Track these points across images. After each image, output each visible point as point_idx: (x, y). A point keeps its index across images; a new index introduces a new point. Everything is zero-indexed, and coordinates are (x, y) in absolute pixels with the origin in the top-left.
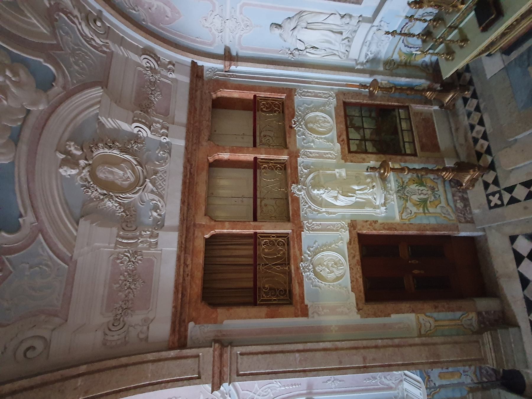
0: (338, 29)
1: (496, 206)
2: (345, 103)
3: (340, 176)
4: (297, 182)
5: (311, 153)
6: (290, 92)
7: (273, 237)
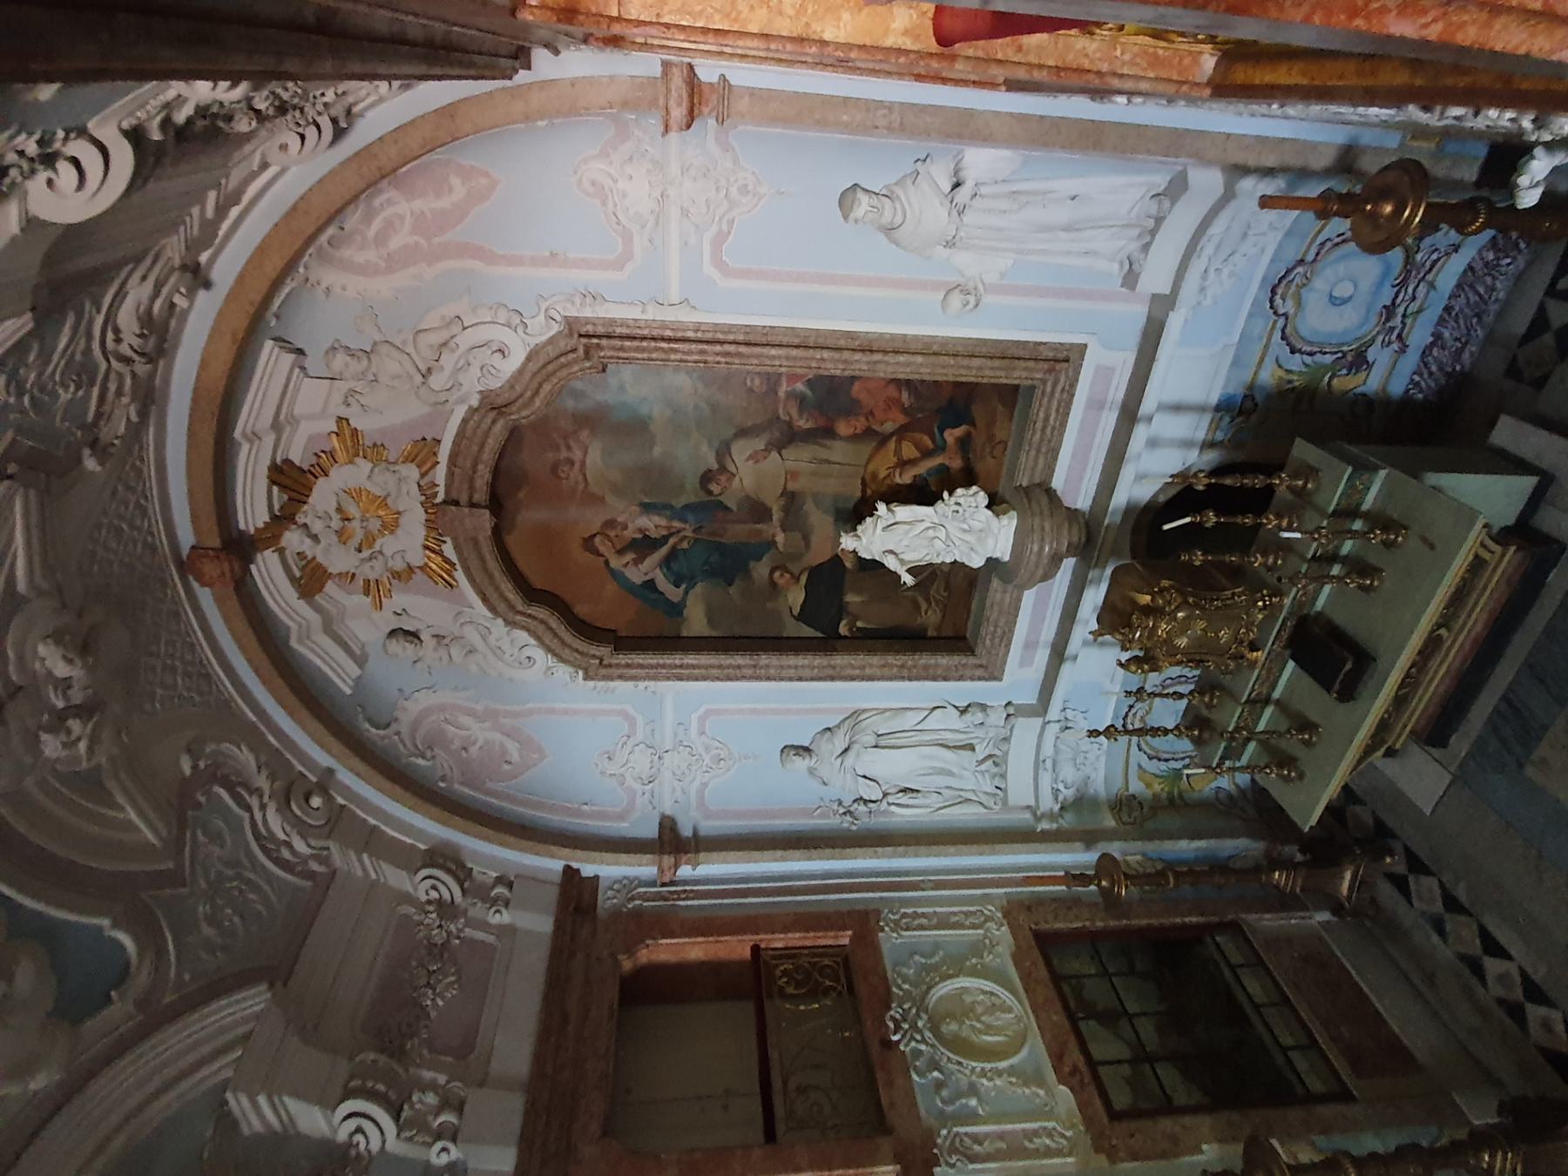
0: (962, 739)
6: (864, 922)
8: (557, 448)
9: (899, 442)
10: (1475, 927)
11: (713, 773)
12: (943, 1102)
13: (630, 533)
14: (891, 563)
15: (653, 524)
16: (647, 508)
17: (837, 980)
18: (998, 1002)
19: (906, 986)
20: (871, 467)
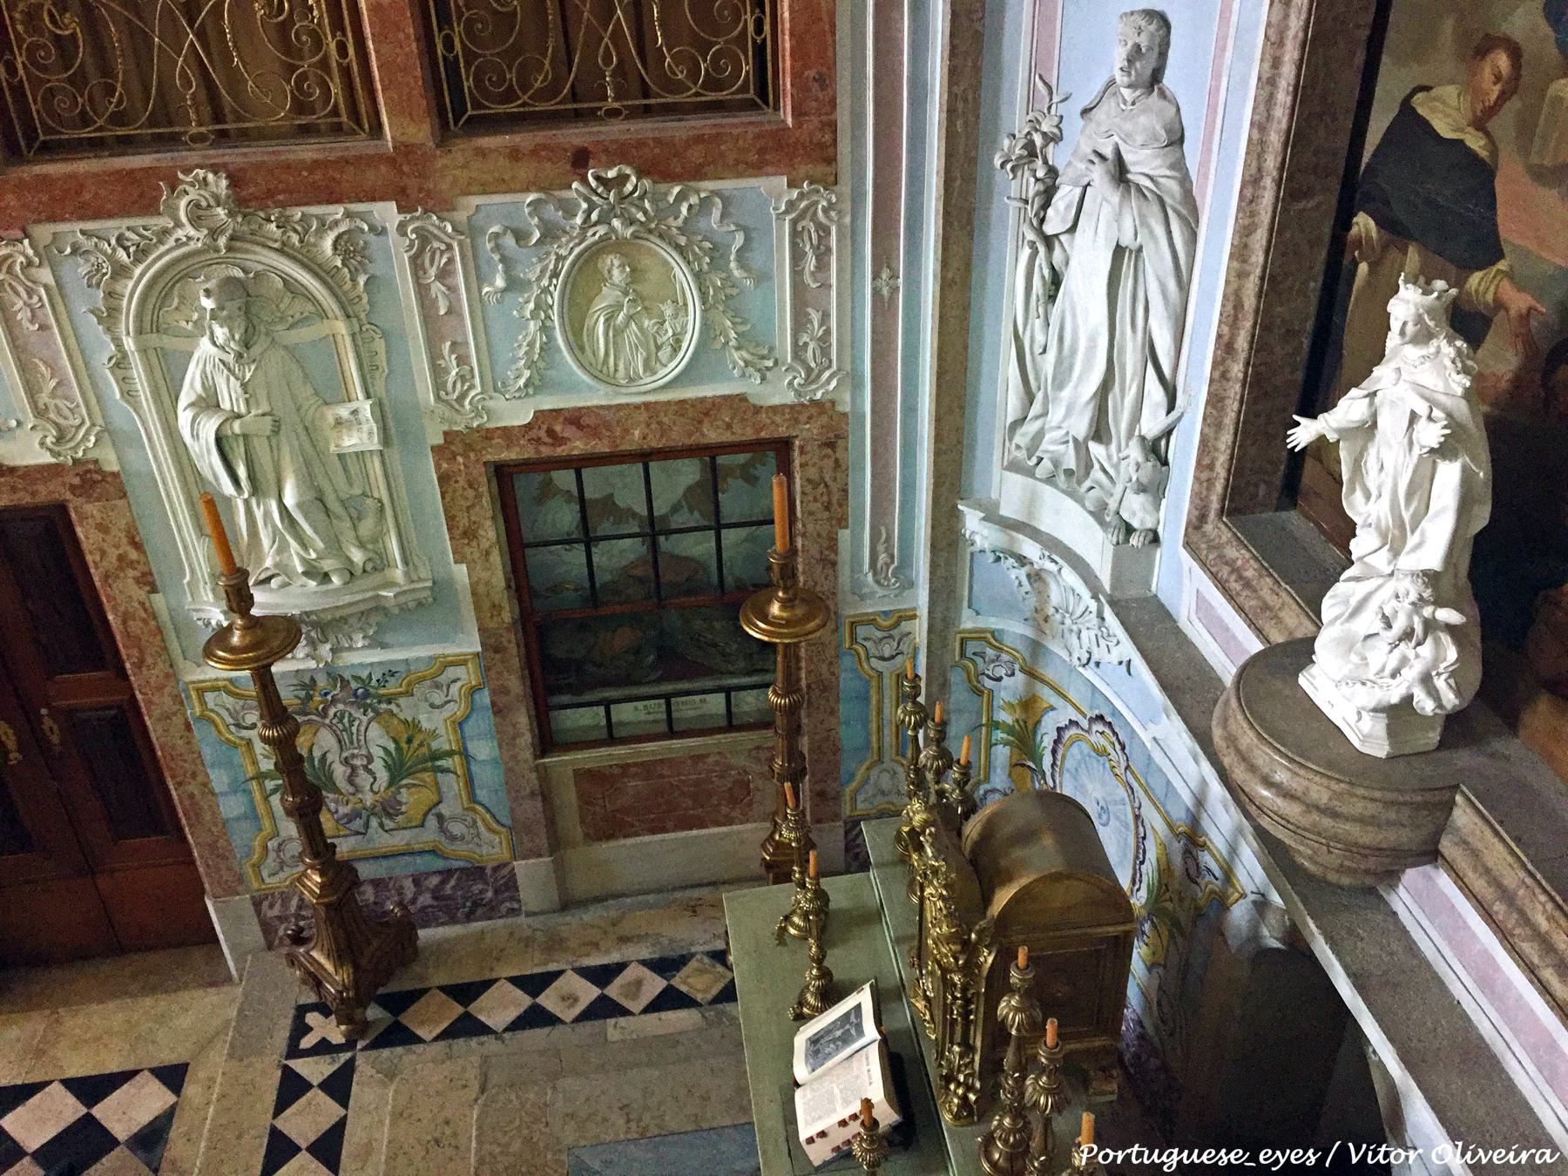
0: (1119, 422)
1: (300, 1029)
2: (783, 447)
3: (339, 422)
4: (247, 194)
5: (444, 274)
6: (812, 153)
7: (342, 49)
10: (699, 997)
12: (496, 236)
14: (1349, 409)
17: (713, 84)
18: (664, 354)
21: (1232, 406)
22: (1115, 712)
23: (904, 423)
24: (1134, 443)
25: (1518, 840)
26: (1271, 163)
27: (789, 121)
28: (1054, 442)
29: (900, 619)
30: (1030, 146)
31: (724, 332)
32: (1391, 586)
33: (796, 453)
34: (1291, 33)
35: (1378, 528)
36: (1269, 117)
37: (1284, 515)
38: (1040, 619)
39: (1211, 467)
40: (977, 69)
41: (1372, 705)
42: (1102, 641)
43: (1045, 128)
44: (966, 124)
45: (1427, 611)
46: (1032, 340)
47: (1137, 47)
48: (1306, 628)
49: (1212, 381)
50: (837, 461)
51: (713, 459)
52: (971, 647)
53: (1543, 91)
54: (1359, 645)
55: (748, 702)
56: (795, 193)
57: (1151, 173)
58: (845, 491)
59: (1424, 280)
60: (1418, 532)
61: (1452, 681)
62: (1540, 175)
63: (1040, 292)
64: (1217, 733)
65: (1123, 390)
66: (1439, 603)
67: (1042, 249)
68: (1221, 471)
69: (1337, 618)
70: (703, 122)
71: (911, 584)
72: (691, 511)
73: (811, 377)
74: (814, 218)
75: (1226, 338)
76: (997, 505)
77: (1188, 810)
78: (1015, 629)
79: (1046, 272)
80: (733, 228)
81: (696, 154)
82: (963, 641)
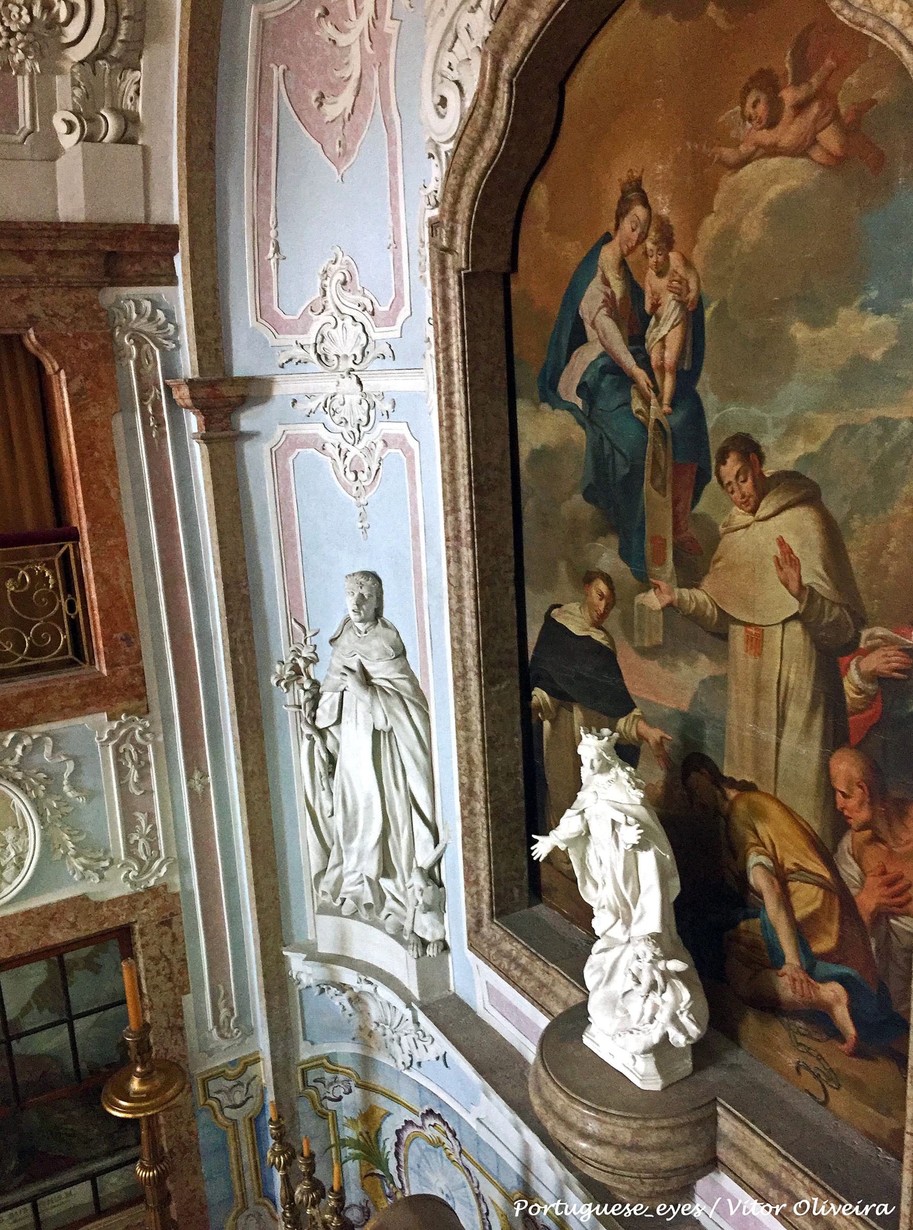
0: (400, 859)
2: (124, 934)
6: (127, 691)
7: (72, 606)
8: (801, 76)
9: (820, 883)
11: (339, 462)
13: (652, 283)
14: (568, 825)
15: (666, 334)
16: (693, 320)
17: (35, 651)
19: (19, 751)
20: (774, 810)
21: (482, 834)
22: (442, 1104)
23: (227, 891)
24: (415, 874)
25: (768, 1133)
26: (471, 662)
27: (105, 671)
28: (352, 884)
29: (246, 1066)
30: (296, 668)
31: (63, 845)
32: (630, 951)
33: (137, 936)
34: (466, 579)
35: (610, 908)
36: (463, 634)
37: (535, 908)
38: (365, 1036)
39: (476, 882)
40: (248, 619)
41: (641, 1048)
42: (419, 1043)
43: (304, 654)
44: (246, 659)
45: (661, 965)
46: (321, 809)
47: (362, 596)
48: (576, 997)
49: (463, 818)
50: (174, 935)
51: (61, 957)
52: (312, 1075)
53: (633, 601)
54: (620, 1002)
55: (113, 1183)
56: (115, 725)
57: (388, 677)
58: (184, 960)
59: (593, 727)
60: (638, 905)
61: (691, 1016)
62: (648, 653)
63: (322, 770)
64: (536, 1101)
65: (398, 835)
66: (668, 957)
67: (318, 740)
68: (484, 883)
69: (599, 983)
70: (31, 681)
71: (250, 1031)
72: (41, 1009)
73: (144, 868)
74: (133, 741)
75: (467, 786)
76: (315, 944)
77: (518, 1175)
78: (345, 1049)
79: (324, 755)
80: (63, 758)
81: (26, 707)
82: (304, 1072)
